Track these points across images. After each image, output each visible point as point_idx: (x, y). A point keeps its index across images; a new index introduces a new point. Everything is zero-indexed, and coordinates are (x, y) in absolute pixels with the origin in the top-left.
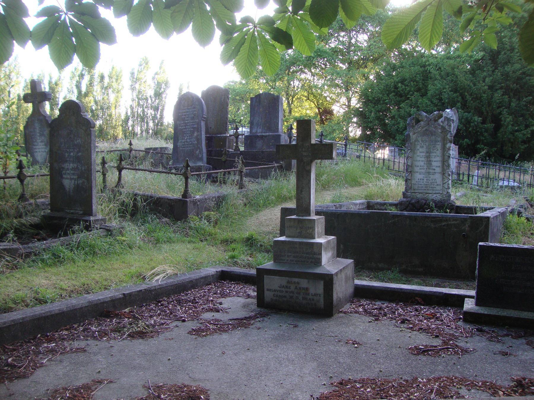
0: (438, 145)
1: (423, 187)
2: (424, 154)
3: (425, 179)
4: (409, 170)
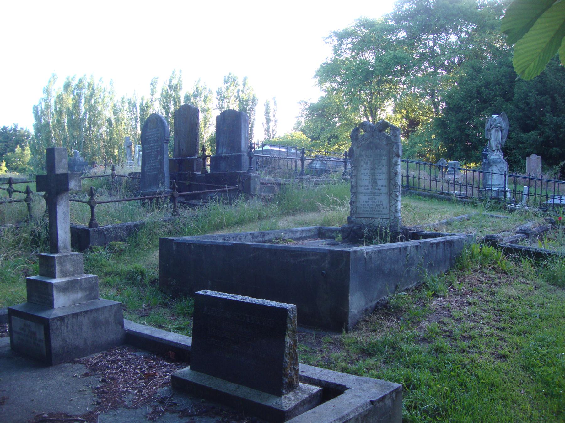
0: (384, 159)
1: (368, 211)
2: (368, 171)
3: (370, 201)
4: (353, 192)
